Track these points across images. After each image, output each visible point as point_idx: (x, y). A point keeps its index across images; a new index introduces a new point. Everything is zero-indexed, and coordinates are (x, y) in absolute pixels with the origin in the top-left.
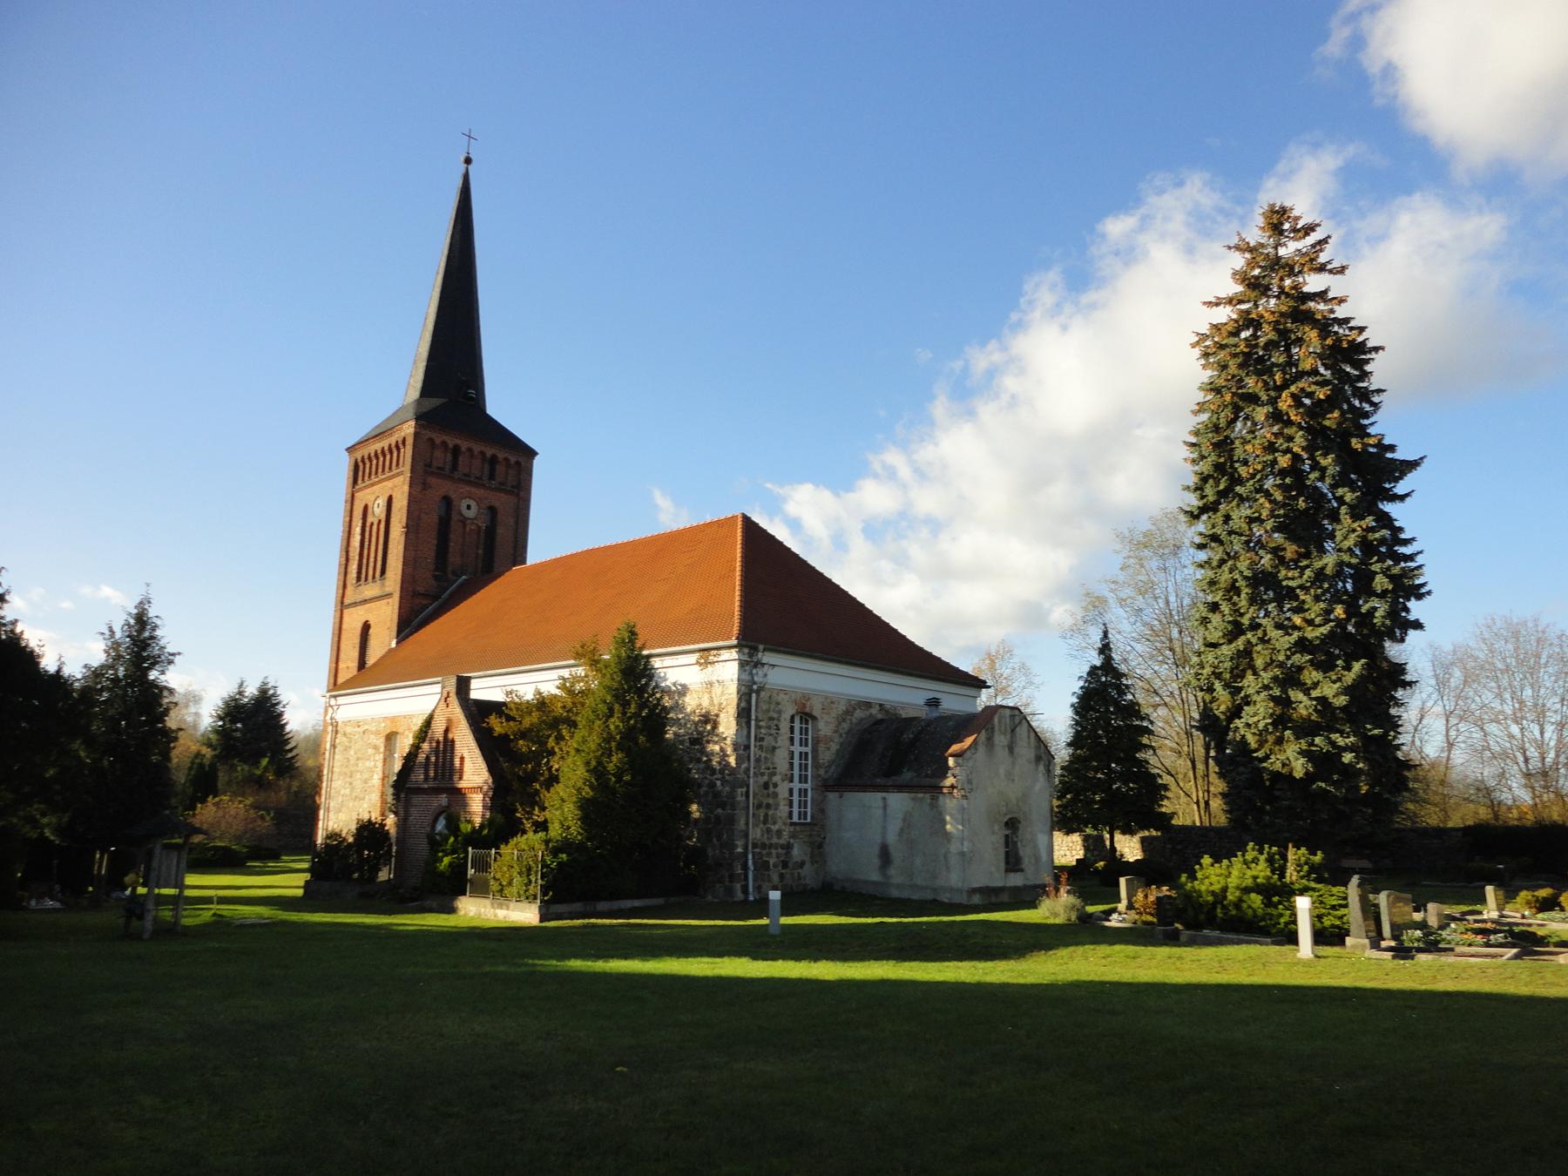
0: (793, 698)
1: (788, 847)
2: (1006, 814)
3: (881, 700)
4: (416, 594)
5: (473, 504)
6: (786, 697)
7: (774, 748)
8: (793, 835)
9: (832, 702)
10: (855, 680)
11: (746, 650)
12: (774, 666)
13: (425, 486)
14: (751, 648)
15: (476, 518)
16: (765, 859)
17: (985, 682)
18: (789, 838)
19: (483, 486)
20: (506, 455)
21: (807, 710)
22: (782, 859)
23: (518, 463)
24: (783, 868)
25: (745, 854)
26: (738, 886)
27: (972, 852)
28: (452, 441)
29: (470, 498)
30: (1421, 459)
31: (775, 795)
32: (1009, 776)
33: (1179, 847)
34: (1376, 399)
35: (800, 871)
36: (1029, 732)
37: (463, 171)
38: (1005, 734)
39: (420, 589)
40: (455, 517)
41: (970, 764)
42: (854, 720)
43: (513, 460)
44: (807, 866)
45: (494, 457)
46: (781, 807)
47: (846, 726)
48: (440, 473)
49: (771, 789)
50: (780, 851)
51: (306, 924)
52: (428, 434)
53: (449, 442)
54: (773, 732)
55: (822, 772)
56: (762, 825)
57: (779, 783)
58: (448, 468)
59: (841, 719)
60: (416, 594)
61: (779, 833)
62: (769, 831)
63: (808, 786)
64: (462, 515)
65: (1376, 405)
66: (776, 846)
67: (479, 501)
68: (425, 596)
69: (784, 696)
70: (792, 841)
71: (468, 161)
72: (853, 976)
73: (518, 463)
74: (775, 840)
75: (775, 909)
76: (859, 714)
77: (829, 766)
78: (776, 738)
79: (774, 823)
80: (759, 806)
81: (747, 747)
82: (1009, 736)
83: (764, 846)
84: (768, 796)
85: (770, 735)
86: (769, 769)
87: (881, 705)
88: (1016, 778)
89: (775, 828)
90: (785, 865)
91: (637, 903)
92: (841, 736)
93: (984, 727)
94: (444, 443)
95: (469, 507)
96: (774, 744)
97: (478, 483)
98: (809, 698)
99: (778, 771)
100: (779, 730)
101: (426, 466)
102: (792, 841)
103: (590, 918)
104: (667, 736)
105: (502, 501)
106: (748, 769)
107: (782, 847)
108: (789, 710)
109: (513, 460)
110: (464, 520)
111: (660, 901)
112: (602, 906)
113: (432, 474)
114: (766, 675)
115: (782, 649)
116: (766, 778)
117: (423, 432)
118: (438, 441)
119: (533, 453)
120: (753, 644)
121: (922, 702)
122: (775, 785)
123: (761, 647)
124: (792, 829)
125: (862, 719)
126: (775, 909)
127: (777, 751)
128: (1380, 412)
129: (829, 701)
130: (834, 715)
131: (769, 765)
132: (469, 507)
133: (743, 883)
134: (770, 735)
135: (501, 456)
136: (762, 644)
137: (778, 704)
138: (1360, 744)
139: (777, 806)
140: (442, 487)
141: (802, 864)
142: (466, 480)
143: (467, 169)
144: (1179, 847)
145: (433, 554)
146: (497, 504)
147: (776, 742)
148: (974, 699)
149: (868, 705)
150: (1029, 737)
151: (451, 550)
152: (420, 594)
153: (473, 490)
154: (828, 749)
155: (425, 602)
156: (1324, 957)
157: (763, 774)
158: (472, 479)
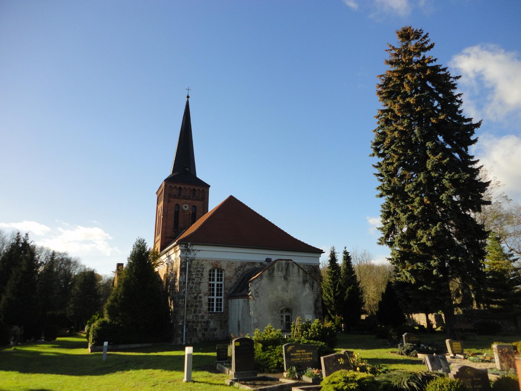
0: (210, 263)
1: (208, 322)
2: (281, 307)
3: (260, 261)
4: (166, 238)
5: (187, 206)
6: (207, 262)
7: (200, 283)
8: (211, 318)
9: (232, 263)
10: (241, 253)
11: (184, 245)
12: (200, 250)
13: (169, 201)
14: (185, 244)
15: (188, 210)
16: (194, 327)
17: (322, 250)
18: (208, 319)
19: (190, 199)
20: (180, 186)
21: (219, 267)
22: (204, 327)
23: (203, 190)
24: (204, 331)
25: (182, 326)
26: (179, 339)
27: (257, 323)
28: (178, 186)
29: (186, 204)
30: (480, 122)
31: (200, 302)
32: (284, 289)
33: (470, 319)
34: (459, 99)
35: (214, 332)
36: (299, 270)
37: (187, 100)
38: (282, 271)
39: (168, 236)
40: (181, 211)
41: (257, 285)
42: (245, 270)
43: (201, 189)
44: (218, 330)
45: (194, 189)
46: (204, 306)
47: (240, 272)
48: (175, 197)
49: (198, 299)
50: (203, 324)
51: (145, 352)
52: (170, 185)
53: (177, 186)
54: (199, 276)
55: (227, 292)
56: (193, 314)
57: (202, 296)
58: (177, 195)
59: (237, 270)
60: (166, 238)
61: (202, 317)
62: (197, 316)
63: (222, 297)
64: (183, 210)
65: (460, 102)
66: (201, 322)
67: (189, 204)
68: (170, 238)
69: (205, 262)
70: (209, 320)
71: (188, 97)
72: (277, 374)
73: (203, 190)
74: (200, 320)
75: (105, 349)
76: (248, 267)
77: (231, 289)
78: (201, 279)
79: (200, 313)
80: (192, 306)
81: (185, 283)
82: (284, 272)
83: (194, 322)
84: (197, 302)
85: (198, 278)
86: (197, 291)
87: (261, 263)
88: (289, 291)
89: (200, 315)
90: (206, 330)
91: (138, 345)
92: (238, 276)
93: (268, 268)
94: (175, 187)
95: (186, 207)
96: (200, 281)
97: (189, 198)
98: (219, 262)
99: (202, 291)
100: (203, 275)
101: (169, 195)
102: (209, 320)
103: (99, 351)
104: (413, 282)
105: (198, 204)
106: (184, 292)
107: (204, 322)
108: (209, 268)
109: (201, 189)
110: (184, 211)
111: (151, 344)
112: (121, 347)
113: (172, 197)
114: (195, 254)
115: (225, 245)
116: (195, 295)
117: (168, 184)
118: (173, 186)
119: (209, 186)
120: (186, 243)
121: (264, 260)
122: (201, 297)
123: (189, 244)
124: (210, 315)
125: (249, 269)
126: (105, 349)
127: (201, 284)
128: (463, 104)
129: (230, 263)
130: (234, 268)
131: (197, 289)
132: (186, 207)
133: (181, 337)
134: (198, 278)
135: (183, 187)
136: (189, 242)
137: (202, 265)
138: (29, 258)
139: (201, 306)
140: (175, 201)
141: (215, 329)
142: (185, 198)
143: (188, 100)
144: (470, 319)
145: (173, 224)
146: (196, 205)
147: (201, 280)
148: (317, 258)
149: (254, 263)
150: (299, 272)
151: (179, 222)
152: (168, 237)
153: (187, 201)
154: (231, 282)
155: (171, 240)
156: (197, 382)
157: (194, 293)
158: (186, 197)
